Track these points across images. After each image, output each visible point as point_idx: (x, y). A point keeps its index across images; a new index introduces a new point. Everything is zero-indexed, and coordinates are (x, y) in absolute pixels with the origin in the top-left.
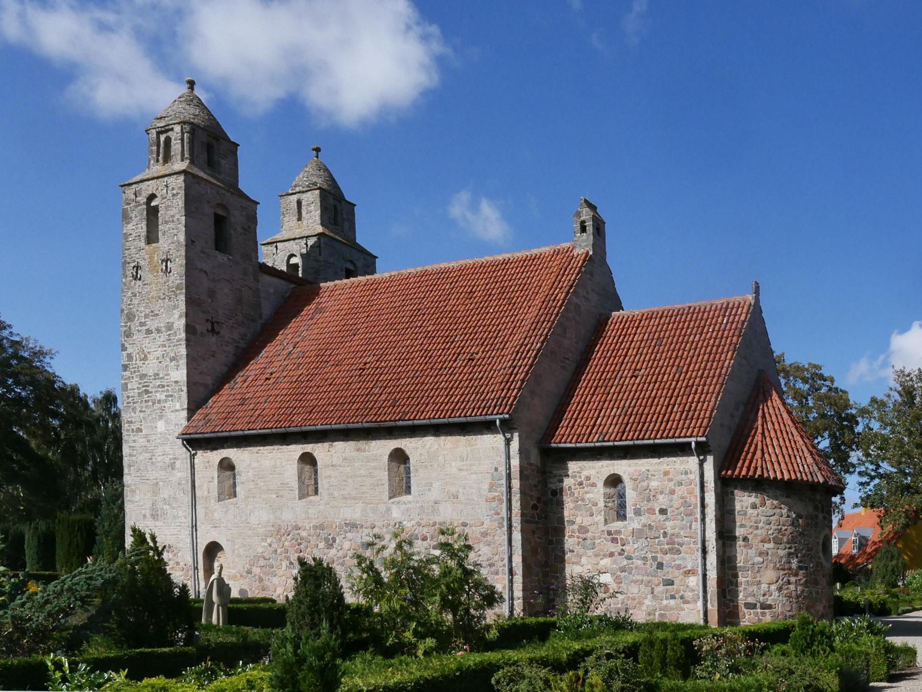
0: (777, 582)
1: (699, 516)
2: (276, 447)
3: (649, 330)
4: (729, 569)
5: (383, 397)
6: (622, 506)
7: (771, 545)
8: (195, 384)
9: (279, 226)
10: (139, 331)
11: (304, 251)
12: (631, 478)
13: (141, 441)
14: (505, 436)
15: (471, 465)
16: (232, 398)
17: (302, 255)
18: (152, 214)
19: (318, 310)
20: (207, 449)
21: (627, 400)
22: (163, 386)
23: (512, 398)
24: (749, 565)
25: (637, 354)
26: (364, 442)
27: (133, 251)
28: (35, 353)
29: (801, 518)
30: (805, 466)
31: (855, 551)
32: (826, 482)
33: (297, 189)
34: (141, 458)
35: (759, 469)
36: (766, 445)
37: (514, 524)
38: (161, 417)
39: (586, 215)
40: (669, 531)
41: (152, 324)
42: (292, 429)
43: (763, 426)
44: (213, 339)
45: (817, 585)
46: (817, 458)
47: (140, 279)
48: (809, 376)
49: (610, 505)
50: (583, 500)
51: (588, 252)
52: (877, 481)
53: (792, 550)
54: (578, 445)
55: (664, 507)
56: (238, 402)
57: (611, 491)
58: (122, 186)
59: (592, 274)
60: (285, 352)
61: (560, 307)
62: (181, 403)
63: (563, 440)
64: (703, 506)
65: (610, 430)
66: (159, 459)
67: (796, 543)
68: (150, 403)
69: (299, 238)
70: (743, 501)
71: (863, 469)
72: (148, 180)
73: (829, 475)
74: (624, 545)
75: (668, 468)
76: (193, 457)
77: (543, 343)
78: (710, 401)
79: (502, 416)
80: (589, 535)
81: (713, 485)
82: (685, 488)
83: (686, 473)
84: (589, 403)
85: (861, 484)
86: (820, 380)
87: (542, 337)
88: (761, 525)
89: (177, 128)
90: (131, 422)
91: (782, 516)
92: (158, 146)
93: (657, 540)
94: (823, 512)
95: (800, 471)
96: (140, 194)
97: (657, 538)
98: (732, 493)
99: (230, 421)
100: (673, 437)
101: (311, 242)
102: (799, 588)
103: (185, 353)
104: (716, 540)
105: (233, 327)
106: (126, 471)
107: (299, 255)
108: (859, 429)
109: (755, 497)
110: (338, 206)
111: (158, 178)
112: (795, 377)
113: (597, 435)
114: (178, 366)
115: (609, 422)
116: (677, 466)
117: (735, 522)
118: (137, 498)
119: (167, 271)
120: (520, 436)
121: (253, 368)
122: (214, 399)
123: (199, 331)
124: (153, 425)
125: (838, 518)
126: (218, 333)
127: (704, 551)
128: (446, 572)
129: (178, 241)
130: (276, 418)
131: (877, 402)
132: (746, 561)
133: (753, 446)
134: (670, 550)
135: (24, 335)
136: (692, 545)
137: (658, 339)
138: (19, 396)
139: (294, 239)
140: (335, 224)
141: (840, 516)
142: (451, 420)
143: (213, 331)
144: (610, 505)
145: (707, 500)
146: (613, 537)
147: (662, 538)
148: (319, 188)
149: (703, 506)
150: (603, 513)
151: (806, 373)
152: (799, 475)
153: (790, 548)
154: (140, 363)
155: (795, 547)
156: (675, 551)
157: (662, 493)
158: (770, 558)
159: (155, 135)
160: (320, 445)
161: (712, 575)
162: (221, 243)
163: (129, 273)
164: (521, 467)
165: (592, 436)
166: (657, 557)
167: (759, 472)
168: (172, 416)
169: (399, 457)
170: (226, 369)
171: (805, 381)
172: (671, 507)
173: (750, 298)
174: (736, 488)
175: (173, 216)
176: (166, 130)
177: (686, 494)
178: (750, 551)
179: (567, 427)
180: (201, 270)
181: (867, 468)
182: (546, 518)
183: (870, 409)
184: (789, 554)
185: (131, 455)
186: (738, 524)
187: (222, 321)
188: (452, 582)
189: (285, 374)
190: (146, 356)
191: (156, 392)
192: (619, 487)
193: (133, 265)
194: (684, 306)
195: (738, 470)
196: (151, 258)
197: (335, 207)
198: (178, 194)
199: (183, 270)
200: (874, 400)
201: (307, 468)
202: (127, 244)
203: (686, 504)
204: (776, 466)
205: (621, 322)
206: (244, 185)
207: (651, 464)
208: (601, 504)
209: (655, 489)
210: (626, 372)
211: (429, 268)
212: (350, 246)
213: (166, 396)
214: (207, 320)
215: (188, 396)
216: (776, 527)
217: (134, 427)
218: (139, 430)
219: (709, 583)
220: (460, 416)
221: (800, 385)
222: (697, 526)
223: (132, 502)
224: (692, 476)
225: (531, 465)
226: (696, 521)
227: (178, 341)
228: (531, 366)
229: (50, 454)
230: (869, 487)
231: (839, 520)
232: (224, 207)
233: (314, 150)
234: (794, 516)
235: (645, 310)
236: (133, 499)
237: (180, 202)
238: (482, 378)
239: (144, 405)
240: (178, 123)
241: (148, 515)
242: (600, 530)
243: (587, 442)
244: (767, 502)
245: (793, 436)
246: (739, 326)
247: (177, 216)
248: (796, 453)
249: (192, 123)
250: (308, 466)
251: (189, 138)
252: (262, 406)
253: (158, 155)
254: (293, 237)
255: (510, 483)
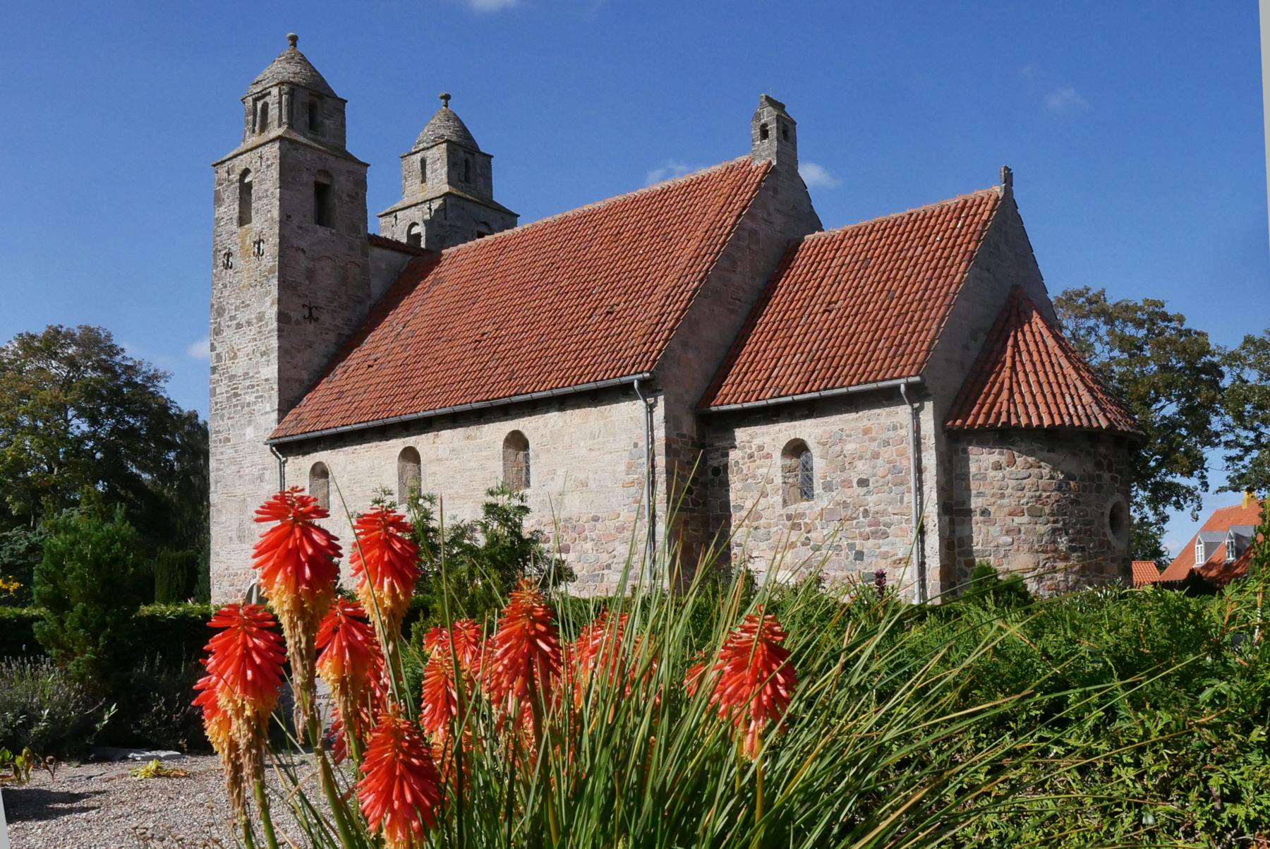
0: (1034, 569)
1: (912, 484)
2: (374, 444)
3: (852, 251)
4: (959, 554)
5: (500, 370)
6: (809, 479)
7: (1026, 519)
8: (288, 380)
9: (400, 194)
10: (228, 326)
11: (427, 217)
12: (818, 443)
13: (229, 452)
14: (646, 401)
15: (604, 443)
16: (329, 392)
17: (425, 222)
18: (245, 190)
19: (437, 281)
20: (298, 454)
21: (815, 342)
22: (253, 386)
23: (656, 352)
24: (991, 547)
25: (834, 282)
26: (474, 428)
27: (225, 236)
28: (149, 378)
29: (1073, 479)
30: (1079, 407)
31: (1231, 559)
32: (1111, 426)
33: (421, 146)
34: (228, 471)
35: (1004, 415)
36: (1018, 382)
37: (658, 513)
38: (250, 422)
39: (768, 116)
40: (872, 508)
41: (242, 317)
42: (391, 420)
43: (1013, 357)
44: (311, 327)
45: (1102, 572)
46: (1100, 396)
47: (231, 268)
48: (1145, 317)
49: (791, 480)
50: (754, 477)
51: (770, 163)
52: (1255, 453)
53: (1059, 525)
54: (746, 405)
55: (865, 477)
56: (334, 396)
57: (793, 462)
58: (214, 165)
59: (775, 190)
60: (395, 333)
61: (728, 235)
62: (271, 403)
63: (728, 400)
64: (919, 470)
65: (789, 382)
66: (247, 471)
67: (1065, 514)
68: (239, 408)
69: (422, 203)
70: (981, 460)
71: (1231, 437)
72: (241, 154)
73: (1119, 417)
74: (809, 532)
75: (869, 424)
76: (282, 464)
77: (701, 281)
78: (929, 330)
79: (641, 376)
80: (762, 522)
81: (933, 440)
82: (894, 449)
83: (895, 428)
84: (765, 351)
85: (1229, 459)
86: (1163, 321)
87: (702, 274)
88: (1007, 492)
89: (275, 91)
90: (219, 432)
91: (1042, 478)
92: (255, 115)
93: (855, 522)
94: (1110, 471)
95: (1069, 414)
96: (233, 171)
97: (855, 518)
98: (965, 451)
99: (323, 419)
100: (875, 381)
101: (435, 205)
102: (1071, 578)
103: (277, 346)
104: (939, 515)
105: (335, 312)
106: (212, 488)
107: (421, 223)
108: (1226, 382)
109: (999, 454)
110: (471, 160)
111: (252, 150)
112: (1125, 321)
113: (772, 390)
114: (268, 361)
115: (789, 372)
116: (882, 420)
117: (970, 490)
118: (223, 518)
119: (259, 254)
120: (666, 400)
121: (356, 357)
122: (309, 396)
123: (294, 319)
124: (242, 432)
125: (1191, 508)
126: (317, 320)
127: (922, 532)
128: (494, 540)
129: (272, 218)
130: (374, 409)
131: (1254, 343)
132: (986, 542)
133: (997, 385)
134: (873, 533)
135: (137, 359)
136: (904, 524)
137: (864, 261)
138: (132, 428)
139: (416, 205)
140: (467, 180)
141: (1195, 505)
142: (577, 388)
143: (311, 318)
144: (791, 480)
145: (925, 462)
146: (794, 522)
147: (861, 519)
148: (447, 141)
149: (919, 470)
150: (781, 491)
151: (1139, 313)
152: (1067, 419)
153: (1055, 522)
154: (229, 363)
155: (1063, 520)
156: (879, 534)
157: (861, 458)
158: (1023, 537)
159: (251, 104)
160: (423, 436)
161: (934, 563)
162: (322, 215)
163: (220, 263)
164: (667, 438)
165: (764, 391)
166: (855, 544)
167: (1003, 418)
168: (261, 420)
169: (517, 442)
170: (325, 361)
171: (1139, 324)
172: (874, 475)
173: (998, 190)
174: (970, 444)
175: (267, 191)
176: (263, 95)
177: (894, 457)
178: (992, 529)
179: (733, 384)
180: (298, 249)
181: (1238, 436)
182: (705, 504)
183: (1243, 353)
184: (1054, 531)
185: (218, 470)
186: (973, 492)
187: (322, 305)
188: (500, 553)
189: (389, 358)
190: (235, 354)
191: (245, 393)
192: (803, 458)
193: (223, 252)
194: (902, 214)
195: (971, 418)
196: (243, 242)
197: (466, 161)
198: (272, 164)
199: (276, 250)
200: (1249, 340)
201: (410, 466)
202: (219, 229)
203: (895, 470)
204: (1031, 409)
205: (815, 247)
206: (353, 146)
207: (847, 421)
208: (779, 480)
209: (852, 454)
210: (817, 306)
211: (570, 213)
212: (484, 205)
213: (256, 397)
214: (304, 306)
215: (279, 395)
216: (1032, 494)
217: (221, 437)
218: (228, 440)
219: (928, 574)
220: (588, 382)
221: (1130, 330)
222: (910, 498)
223: (218, 523)
224: (903, 432)
225: (683, 436)
226: (909, 492)
227: (269, 332)
228: (684, 311)
229: (165, 491)
230: (1242, 463)
231: (1194, 510)
232: (325, 173)
233: (442, 98)
234: (1061, 477)
235: (848, 227)
236: (219, 520)
237: (274, 173)
238: (621, 333)
239: (233, 410)
240: (276, 85)
241: (235, 537)
242: (777, 514)
243: (757, 400)
244: (1018, 460)
245: (1061, 368)
246: (979, 228)
247: (272, 190)
248: (1064, 389)
249: (291, 83)
250: (412, 464)
251: (288, 100)
252: (360, 398)
253: (254, 125)
254: (415, 202)
255: (653, 460)
